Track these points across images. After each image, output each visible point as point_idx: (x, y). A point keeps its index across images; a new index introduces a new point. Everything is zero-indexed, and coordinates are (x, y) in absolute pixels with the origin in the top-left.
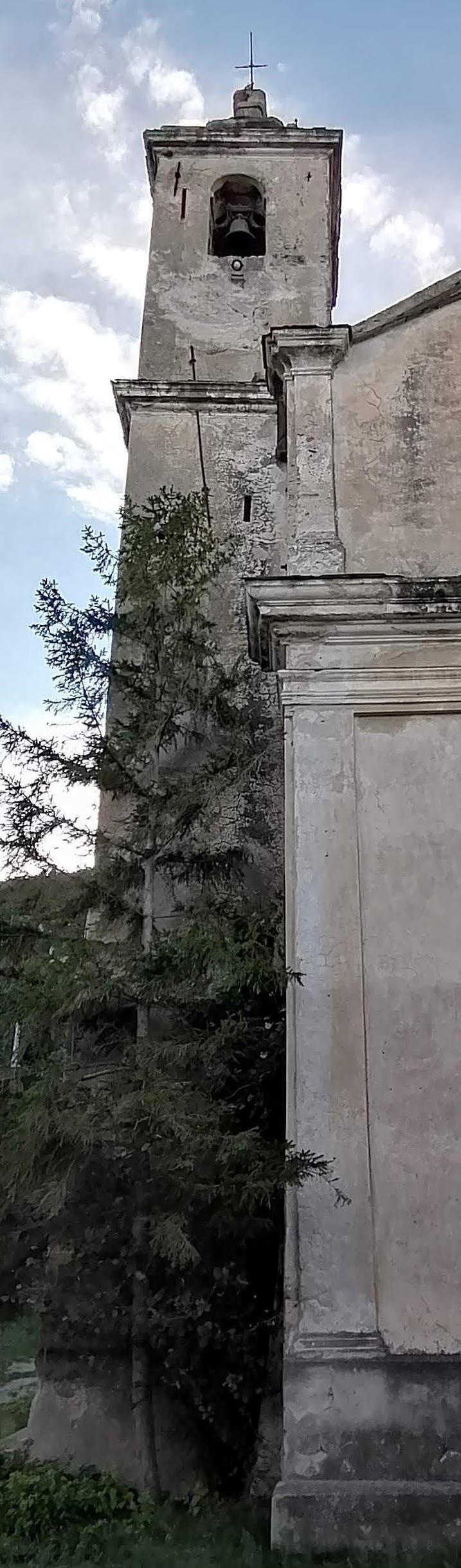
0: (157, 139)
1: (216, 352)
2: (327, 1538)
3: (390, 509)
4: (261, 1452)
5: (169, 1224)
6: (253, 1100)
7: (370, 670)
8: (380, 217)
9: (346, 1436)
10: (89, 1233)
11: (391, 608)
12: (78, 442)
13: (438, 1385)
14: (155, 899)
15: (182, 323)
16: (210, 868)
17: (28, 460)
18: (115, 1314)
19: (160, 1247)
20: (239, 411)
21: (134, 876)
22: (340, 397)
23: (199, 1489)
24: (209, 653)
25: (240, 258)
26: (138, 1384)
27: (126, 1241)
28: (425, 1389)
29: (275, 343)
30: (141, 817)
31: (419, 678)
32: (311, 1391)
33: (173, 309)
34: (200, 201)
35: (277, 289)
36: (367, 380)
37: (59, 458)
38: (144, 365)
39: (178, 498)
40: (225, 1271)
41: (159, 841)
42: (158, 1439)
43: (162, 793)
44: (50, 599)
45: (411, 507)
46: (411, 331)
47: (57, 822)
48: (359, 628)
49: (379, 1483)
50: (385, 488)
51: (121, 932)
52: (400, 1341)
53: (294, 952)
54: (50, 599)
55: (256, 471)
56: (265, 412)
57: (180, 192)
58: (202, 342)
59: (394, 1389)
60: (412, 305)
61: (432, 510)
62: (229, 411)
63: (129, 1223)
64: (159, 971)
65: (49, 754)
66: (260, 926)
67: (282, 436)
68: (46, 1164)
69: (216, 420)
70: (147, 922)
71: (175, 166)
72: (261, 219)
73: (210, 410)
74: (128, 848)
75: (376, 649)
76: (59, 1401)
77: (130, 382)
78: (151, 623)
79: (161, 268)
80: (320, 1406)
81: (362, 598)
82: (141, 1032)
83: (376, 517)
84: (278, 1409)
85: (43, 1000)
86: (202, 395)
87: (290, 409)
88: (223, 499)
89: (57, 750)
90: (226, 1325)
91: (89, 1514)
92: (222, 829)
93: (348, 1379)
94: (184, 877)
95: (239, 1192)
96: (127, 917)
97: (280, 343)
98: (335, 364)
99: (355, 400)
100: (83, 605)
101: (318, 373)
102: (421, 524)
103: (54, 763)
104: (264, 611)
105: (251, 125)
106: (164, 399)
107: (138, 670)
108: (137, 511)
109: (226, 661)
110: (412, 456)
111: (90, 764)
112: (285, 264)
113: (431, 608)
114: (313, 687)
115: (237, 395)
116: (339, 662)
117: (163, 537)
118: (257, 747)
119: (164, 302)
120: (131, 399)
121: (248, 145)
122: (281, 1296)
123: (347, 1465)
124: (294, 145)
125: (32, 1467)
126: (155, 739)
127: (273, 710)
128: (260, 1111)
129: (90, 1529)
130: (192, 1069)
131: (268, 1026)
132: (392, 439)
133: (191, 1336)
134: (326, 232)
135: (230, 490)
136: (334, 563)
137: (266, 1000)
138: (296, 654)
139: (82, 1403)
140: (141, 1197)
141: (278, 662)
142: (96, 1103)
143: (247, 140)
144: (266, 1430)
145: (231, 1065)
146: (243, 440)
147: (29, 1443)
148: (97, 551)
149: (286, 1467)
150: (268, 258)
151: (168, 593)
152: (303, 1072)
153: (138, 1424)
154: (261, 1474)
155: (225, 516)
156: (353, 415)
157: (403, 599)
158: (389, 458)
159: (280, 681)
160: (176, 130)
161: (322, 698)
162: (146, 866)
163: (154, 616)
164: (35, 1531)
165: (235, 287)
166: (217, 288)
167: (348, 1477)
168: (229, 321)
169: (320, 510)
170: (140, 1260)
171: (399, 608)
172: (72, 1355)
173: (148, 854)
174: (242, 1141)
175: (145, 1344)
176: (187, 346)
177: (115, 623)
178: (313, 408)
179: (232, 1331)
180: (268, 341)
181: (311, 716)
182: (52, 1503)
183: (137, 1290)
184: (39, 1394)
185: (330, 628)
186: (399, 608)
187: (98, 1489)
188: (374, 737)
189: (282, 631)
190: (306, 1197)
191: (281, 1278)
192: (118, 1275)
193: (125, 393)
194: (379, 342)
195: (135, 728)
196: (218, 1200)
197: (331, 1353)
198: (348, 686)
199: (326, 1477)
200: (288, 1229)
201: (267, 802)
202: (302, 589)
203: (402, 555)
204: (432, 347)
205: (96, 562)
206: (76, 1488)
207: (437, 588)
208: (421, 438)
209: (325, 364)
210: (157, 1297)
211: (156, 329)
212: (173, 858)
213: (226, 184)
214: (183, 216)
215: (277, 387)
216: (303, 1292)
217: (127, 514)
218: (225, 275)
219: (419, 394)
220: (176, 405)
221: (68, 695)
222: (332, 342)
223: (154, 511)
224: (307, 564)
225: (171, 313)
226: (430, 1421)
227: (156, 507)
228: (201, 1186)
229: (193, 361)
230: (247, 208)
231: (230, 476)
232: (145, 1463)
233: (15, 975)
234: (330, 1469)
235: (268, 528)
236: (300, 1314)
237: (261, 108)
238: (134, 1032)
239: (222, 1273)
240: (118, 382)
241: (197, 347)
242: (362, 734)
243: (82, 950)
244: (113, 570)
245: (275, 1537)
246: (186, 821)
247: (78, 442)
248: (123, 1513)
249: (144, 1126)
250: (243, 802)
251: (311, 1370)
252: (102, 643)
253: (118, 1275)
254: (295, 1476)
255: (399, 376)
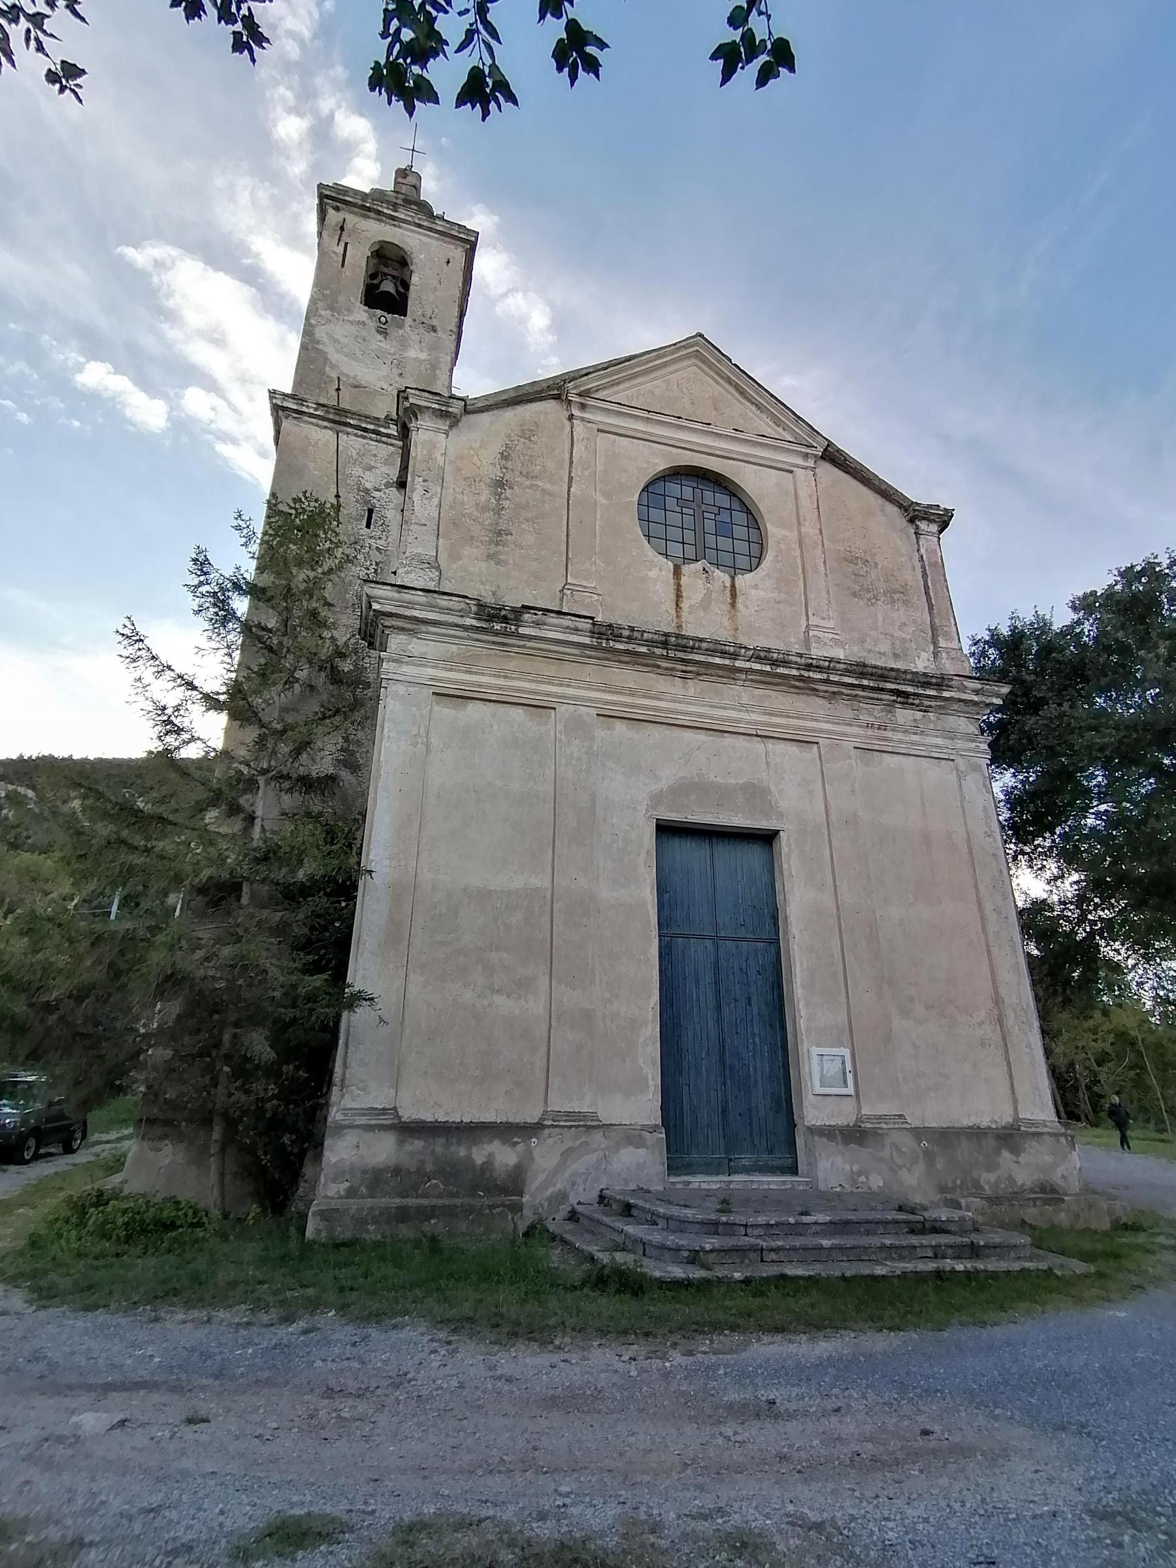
0: (328, 193)
1: (358, 387)
2: (344, 1233)
3: (477, 547)
4: (303, 1184)
5: (254, 1034)
6: (325, 954)
7: (448, 662)
8: (504, 289)
9: (364, 1172)
10: (187, 1039)
11: (469, 621)
12: (230, 404)
13: (431, 1140)
14: (266, 805)
15: (333, 356)
16: (311, 787)
17: (183, 410)
18: (205, 1094)
19: (247, 1049)
20: (371, 439)
21: (251, 785)
22: (451, 453)
23: (255, 1208)
24: (328, 628)
25: (385, 314)
26: (216, 1141)
27: (218, 1045)
28: (422, 1143)
29: (407, 398)
30: (261, 742)
31: (482, 674)
32: (345, 1144)
33: (325, 340)
34: (359, 257)
35: (411, 345)
36: (473, 445)
37: (212, 415)
38: (299, 382)
39: (316, 501)
40: (291, 1067)
41: (273, 763)
42: (228, 1178)
43: (279, 727)
44: (202, 564)
45: (493, 549)
46: (509, 414)
47: (193, 739)
48: (444, 631)
49: (383, 1200)
50: (476, 530)
51: (235, 826)
52: (408, 1113)
53: (368, 854)
54: (202, 564)
55: (379, 490)
56: (392, 445)
57: (342, 244)
58: (347, 376)
59: (401, 1143)
60: (513, 394)
61: (507, 554)
62: (364, 437)
63: (221, 1032)
64: (266, 859)
65: (191, 686)
66: (344, 834)
67: (404, 468)
68: (164, 991)
69: (352, 443)
70: (258, 822)
71: (341, 220)
72: (406, 286)
73: (348, 434)
74: (248, 765)
75: (454, 648)
76: (151, 1155)
77: (284, 394)
78: (285, 599)
79: (320, 304)
80: (348, 1153)
81: (449, 611)
82: (245, 900)
83: (467, 551)
84: (318, 1157)
85: (172, 873)
86: (343, 419)
87: (412, 454)
88: (352, 507)
89: (196, 683)
90: (287, 1102)
91: (172, 1226)
92: (322, 758)
93: (369, 1137)
94: (290, 790)
95: (310, 1015)
96: (242, 816)
97: (411, 400)
98: (451, 427)
99: (462, 458)
100: (228, 572)
101: (437, 431)
102: (498, 563)
103: (195, 693)
104: (375, 606)
105: (408, 202)
106: (311, 415)
107: (270, 631)
108: (282, 507)
109: (342, 636)
110: (499, 510)
111: (222, 698)
112: (421, 330)
113: (497, 627)
114: (405, 669)
115: (371, 427)
116: (426, 653)
117: (297, 530)
118: (357, 704)
119: (320, 333)
120: (284, 409)
121: (404, 221)
122: (330, 1084)
123: (364, 1190)
124: (437, 232)
125: (127, 1198)
126: (280, 687)
127: (371, 677)
128: (330, 961)
129: (173, 1234)
130: (280, 930)
131: (343, 904)
132: (485, 495)
133: (261, 1110)
134: (456, 312)
135: (357, 501)
136: (432, 579)
137: (344, 888)
138: (396, 642)
139: (169, 1154)
140: (233, 1017)
141: (381, 644)
142: (200, 947)
143: (402, 216)
144: (308, 1170)
145: (312, 928)
146: (372, 463)
147: (125, 1181)
148: (245, 531)
149: (320, 1191)
150: (408, 320)
151: (301, 576)
152: (364, 938)
153: (213, 1167)
154: (301, 1198)
155: (351, 526)
156: (459, 470)
157: (478, 616)
158: (484, 509)
159: (381, 660)
160: (346, 190)
161: (410, 673)
162: (261, 780)
163: (288, 593)
164: (128, 1239)
165: (380, 337)
166: (364, 334)
167: (363, 1197)
168: (374, 365)
169: (426, 538)
170: (227, 1058)
171: (475, 623)
172: (167, 1123)
173: (264, 772)
174: (318, 981)
175: (225, 1116)
176: (335, 376)
177: (254, 591)
178: (430, 458)
179: (292, 1106)
180: (402, 395)
181: (401, 689)
182: (142, 1221)
183: (223, 1079)
184: (134, 1149)
185: (423, 628)
186: (475, 623)
187: (179, 1210)
188: (445, 711)
189: (386, 624)
190: (355, 1021)
191: (331, 1073)
192: (209, 1069)
193: (279, 402)
194: (485, 417)
195: (263, 674)
196: (294, 1020)
197: (362, 1121)
198: (431, 672)
199: (348, 1197)
200: (340, 1042)
201: (358, 743)
202: (407, 596)
203: (482, 583)
204: (523, 431)
205: (244, 540)
206: (162, 1210)
207: (503, 613)
208: (507, 499)
209: (443, 425)
210: (238, 1084)
211: (311, 358)
212: (282, 777)
213: (381, 247)
214: (343, 265)
215: (405, 433)
216: (347, 1082)
217: (273, 505)
218: (372, 324)
219: (509, 465)
220: (321, 422)
221: (214, 645)
222: (450, 410)
223: (296, 509)
224: (412, 576)
225: (324, 344)
226: (422, 1162)
227: (298, 506)
228: (283, 1010)
229: (338, 389)
230: (395, 273)
231: (359, 490)
232: (216, 1193)
233: (147, 850)
234: (352, 1192)
235: (384, 537)
236: (343, 1096)
237: (417, 188)
238: (239, 898)
239: (288, 1069)
240: (275, 392)
241: (343, 379)
242: (436, 708)
243: (208, 838)
244: (255, 548)
245: (309, 1234)
246: (297, 752)
247: (230, 404)
248: (199, 1225)
249: (245, 968)
250: (341, 740)
251: (346, 1131)
252: (241, 605)
253: (209, 1069)
254: (326, 1197)
255: (497, 447)
